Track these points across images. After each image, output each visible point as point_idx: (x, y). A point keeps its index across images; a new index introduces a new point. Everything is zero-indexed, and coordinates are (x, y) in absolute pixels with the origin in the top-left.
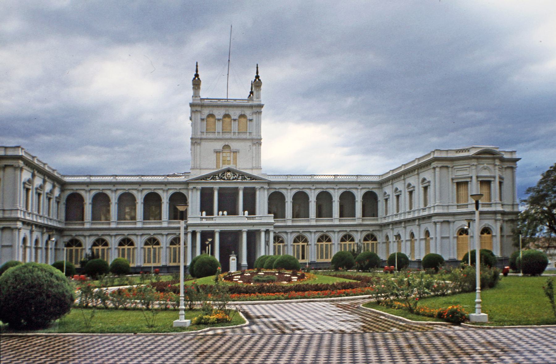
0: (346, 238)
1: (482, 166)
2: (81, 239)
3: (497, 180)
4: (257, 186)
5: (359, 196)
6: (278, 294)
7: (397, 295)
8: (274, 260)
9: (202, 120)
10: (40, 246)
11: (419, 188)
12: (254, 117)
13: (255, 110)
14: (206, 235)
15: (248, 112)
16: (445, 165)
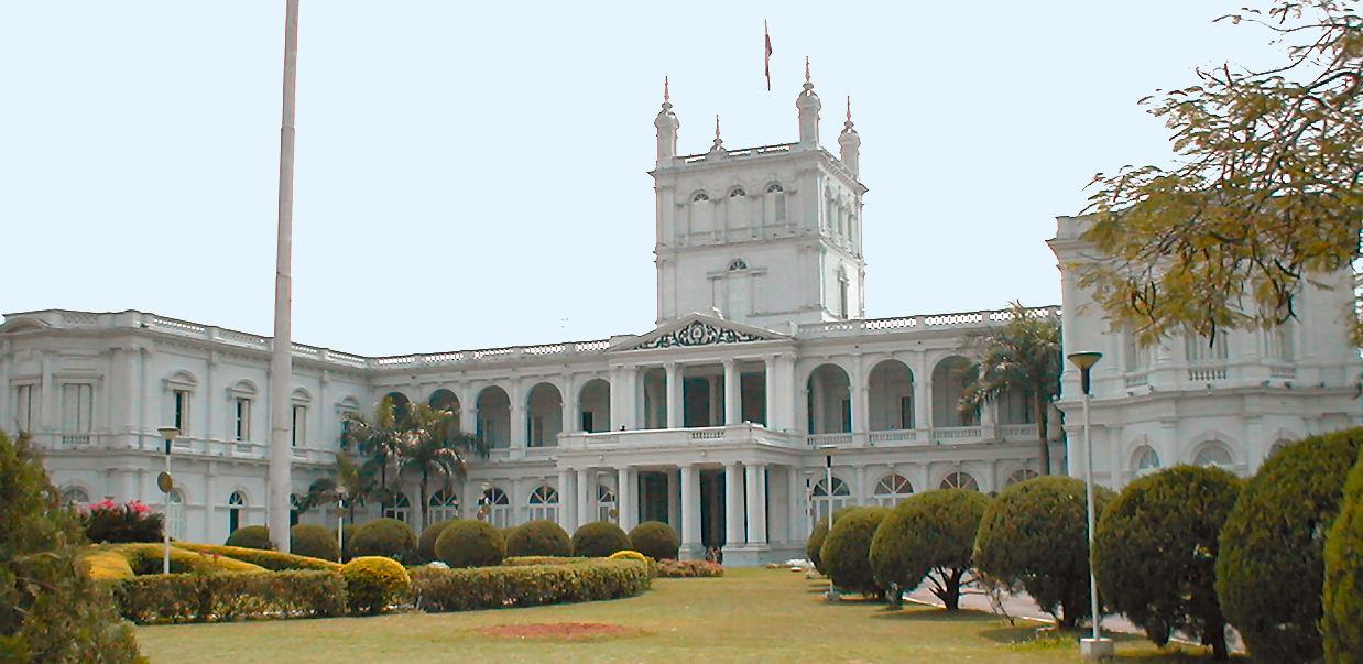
0: (890, 485)
2: (506, 489)
6: (552, 644)
9: (680, 206)
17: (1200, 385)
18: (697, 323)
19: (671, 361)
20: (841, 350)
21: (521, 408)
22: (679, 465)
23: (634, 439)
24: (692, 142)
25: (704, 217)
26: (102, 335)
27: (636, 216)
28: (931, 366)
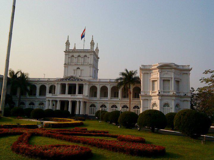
1: (164, 73)
2: (34, 102)
4: (83, 83)
5: (38, 87)
7: (16, 147)
16: (146, 72)
18: (72, 77)
19: (67, 83)
20: (96, 83)
21: (99, 90)
22: (69, 100)
23: (59, 96)
24: (71, 47)
26: (181, 70)
27: (62, 58)
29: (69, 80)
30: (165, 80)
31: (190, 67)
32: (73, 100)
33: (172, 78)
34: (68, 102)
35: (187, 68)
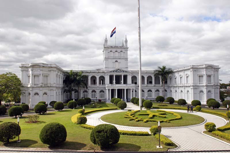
3: (213, 75)
8: (73, 103)
9: (109, 52)
10: (57, 94)
11: (184, 76)
12: (125, 52)
13: (126, 49)
14: (113, 91)
15: (123, 50)
17: (36, 86)
19: (115, 74)
25: (112, 55)
28: (147, 76)
29: (116, 72)
30: (200, 76)
31: (219, 67)
32: (113, 88)
33: (204, 74)
34: (124, 90)
35: (218, 67)
